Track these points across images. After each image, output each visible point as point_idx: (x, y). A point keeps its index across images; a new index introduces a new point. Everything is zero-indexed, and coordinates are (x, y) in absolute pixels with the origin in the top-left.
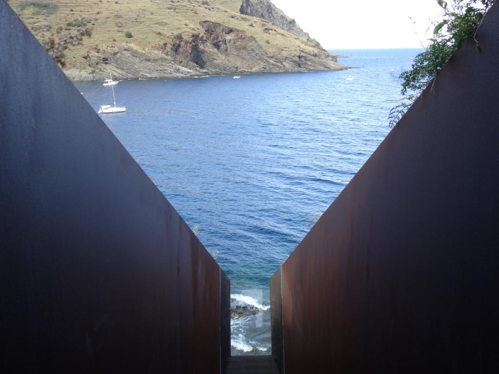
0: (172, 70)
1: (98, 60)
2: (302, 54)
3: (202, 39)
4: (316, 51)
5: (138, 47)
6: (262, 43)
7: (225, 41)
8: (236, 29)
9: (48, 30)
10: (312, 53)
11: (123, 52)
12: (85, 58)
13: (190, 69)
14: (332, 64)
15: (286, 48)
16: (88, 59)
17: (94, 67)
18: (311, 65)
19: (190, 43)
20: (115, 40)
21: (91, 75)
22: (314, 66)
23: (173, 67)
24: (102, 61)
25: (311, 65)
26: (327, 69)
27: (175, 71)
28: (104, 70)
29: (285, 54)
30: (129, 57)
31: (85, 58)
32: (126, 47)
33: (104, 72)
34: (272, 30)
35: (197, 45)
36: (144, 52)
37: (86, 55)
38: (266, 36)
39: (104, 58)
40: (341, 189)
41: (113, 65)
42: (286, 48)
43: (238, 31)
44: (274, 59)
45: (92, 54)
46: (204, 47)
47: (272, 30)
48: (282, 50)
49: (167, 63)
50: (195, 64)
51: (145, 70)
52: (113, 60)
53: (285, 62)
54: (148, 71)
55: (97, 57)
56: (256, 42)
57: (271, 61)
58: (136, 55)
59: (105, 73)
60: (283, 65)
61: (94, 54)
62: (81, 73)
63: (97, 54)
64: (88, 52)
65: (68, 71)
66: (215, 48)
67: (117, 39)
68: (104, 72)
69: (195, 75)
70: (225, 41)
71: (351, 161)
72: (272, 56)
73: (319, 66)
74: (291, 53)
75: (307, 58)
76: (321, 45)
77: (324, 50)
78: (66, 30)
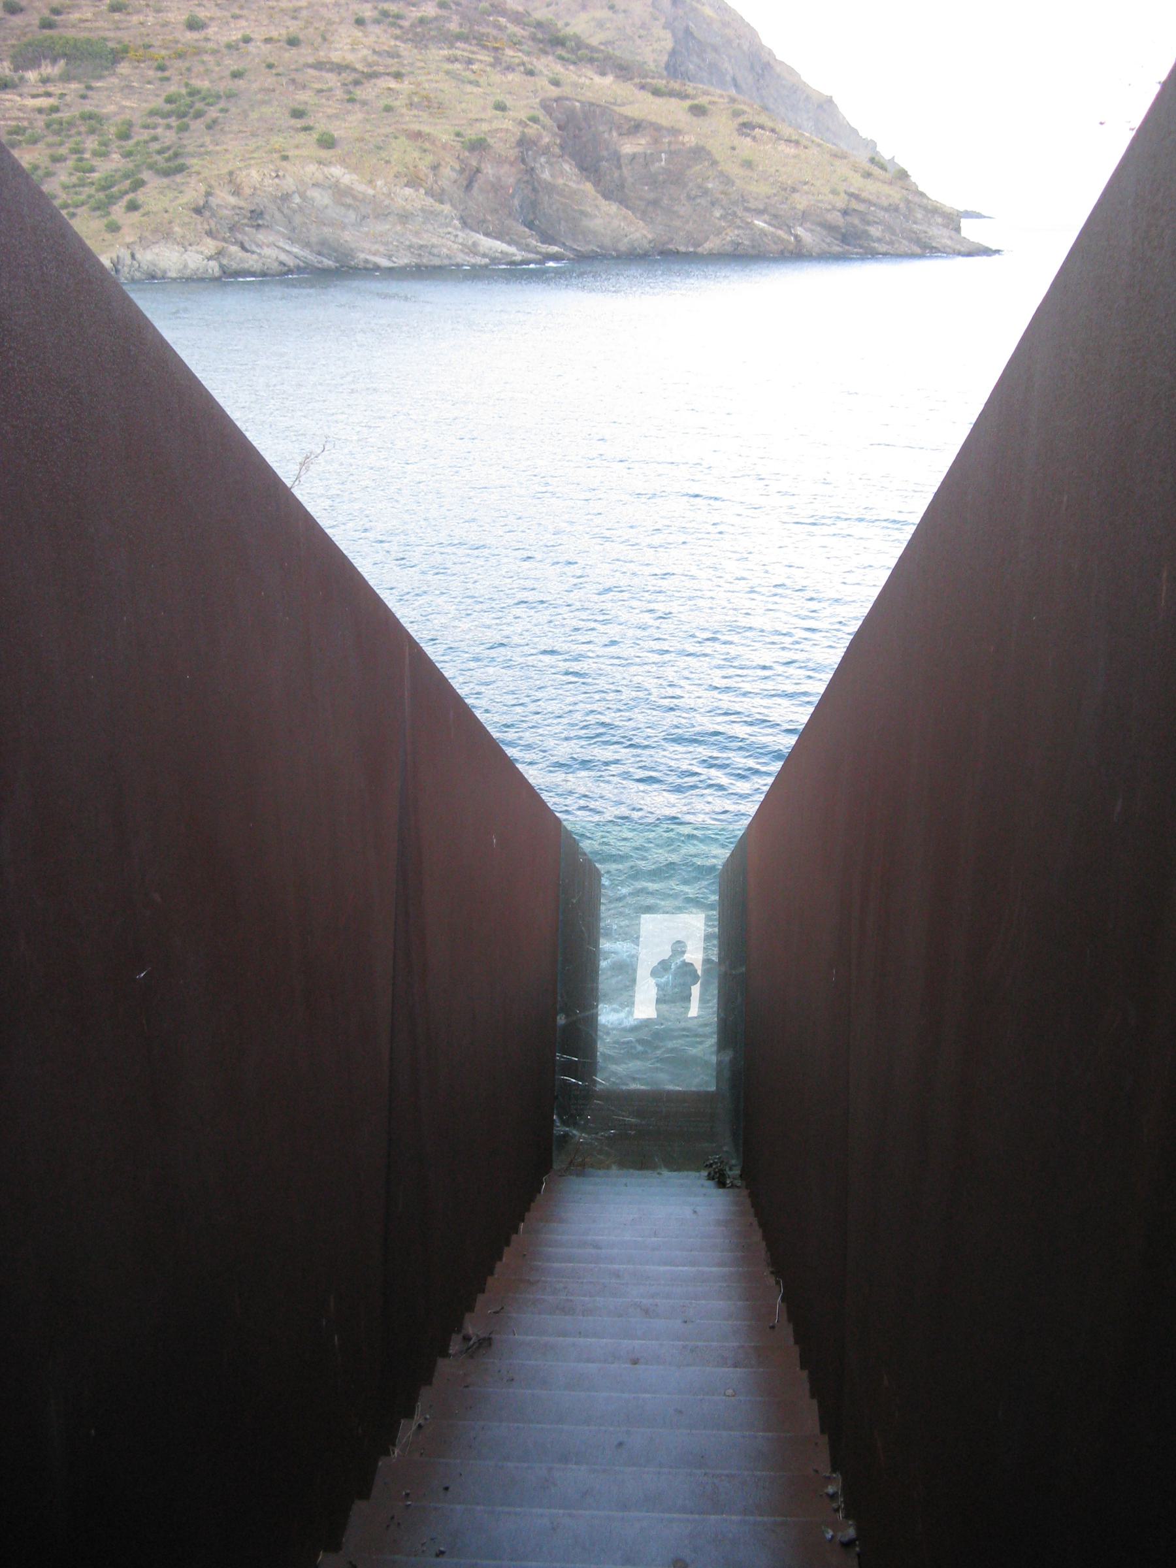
0: (456, 246)
1: (236, 218)
2: (854, 205)
3: (546, 151)
4: (894, 194)
5: (355, 177)
6: (734, 170)
7: (619, 160)
8: (652, 124)
9: (92, 131)
10: (885, 203)
11: (309, 193)
12: (198, 211)
13: (509, 244)
14: (939, 234)
15: (806, 183)
16: (207, 214)
17: (224, 240)
18: (879, 240)
19: (553, 73)
20: (285, 158)
21: (212, 263)
22: (891, 243)
23: (456, 236)
24: (245, 221)
25: (879, 240)
26: (926, 249)
27: (462, 251)
28: (254, 248)
29: (801, 202)
30: (326, 207)
31: (198, 211)
32: (319, 176)
33: (253, 252)
34: (762, 127)
35: (532, 169)
36: (371, 192)
37: (201, 203)
38: (745, 144)
39: (252, 212)
40: (770, 780)
41: (278, 232)
42: (806, 183)
43: (658, 128)
44: (766, 217)
45: (219, 201)
46: (614, 49)
47: (762, 127)
48: (794, 190)
49: (441, 226)
50: (527, 230)
51: (376, 247)
52: (278, 215)
53: (801, 225)
54: (382, 249)
55: (234, 208)
56: (715, 163)
57: (756, 222)
58: (349, 201)
59: (255, 257)
60: (796, 236)
61: (224, 198)
62: (185, 256)
63: (233, 200)
64: (208, 194)
65: (148, 252)
66: (588, 179)
67: (290, 154)
68: (253, 252)
69: (523, 262)
70: (617, 157)
71: (678, 821)
72: (761, 207)
73: (905, 242)
74: (819, 201)
75: (871, 218)
76: (913, 179)
77: (922, 195)
78: (146, 127)
